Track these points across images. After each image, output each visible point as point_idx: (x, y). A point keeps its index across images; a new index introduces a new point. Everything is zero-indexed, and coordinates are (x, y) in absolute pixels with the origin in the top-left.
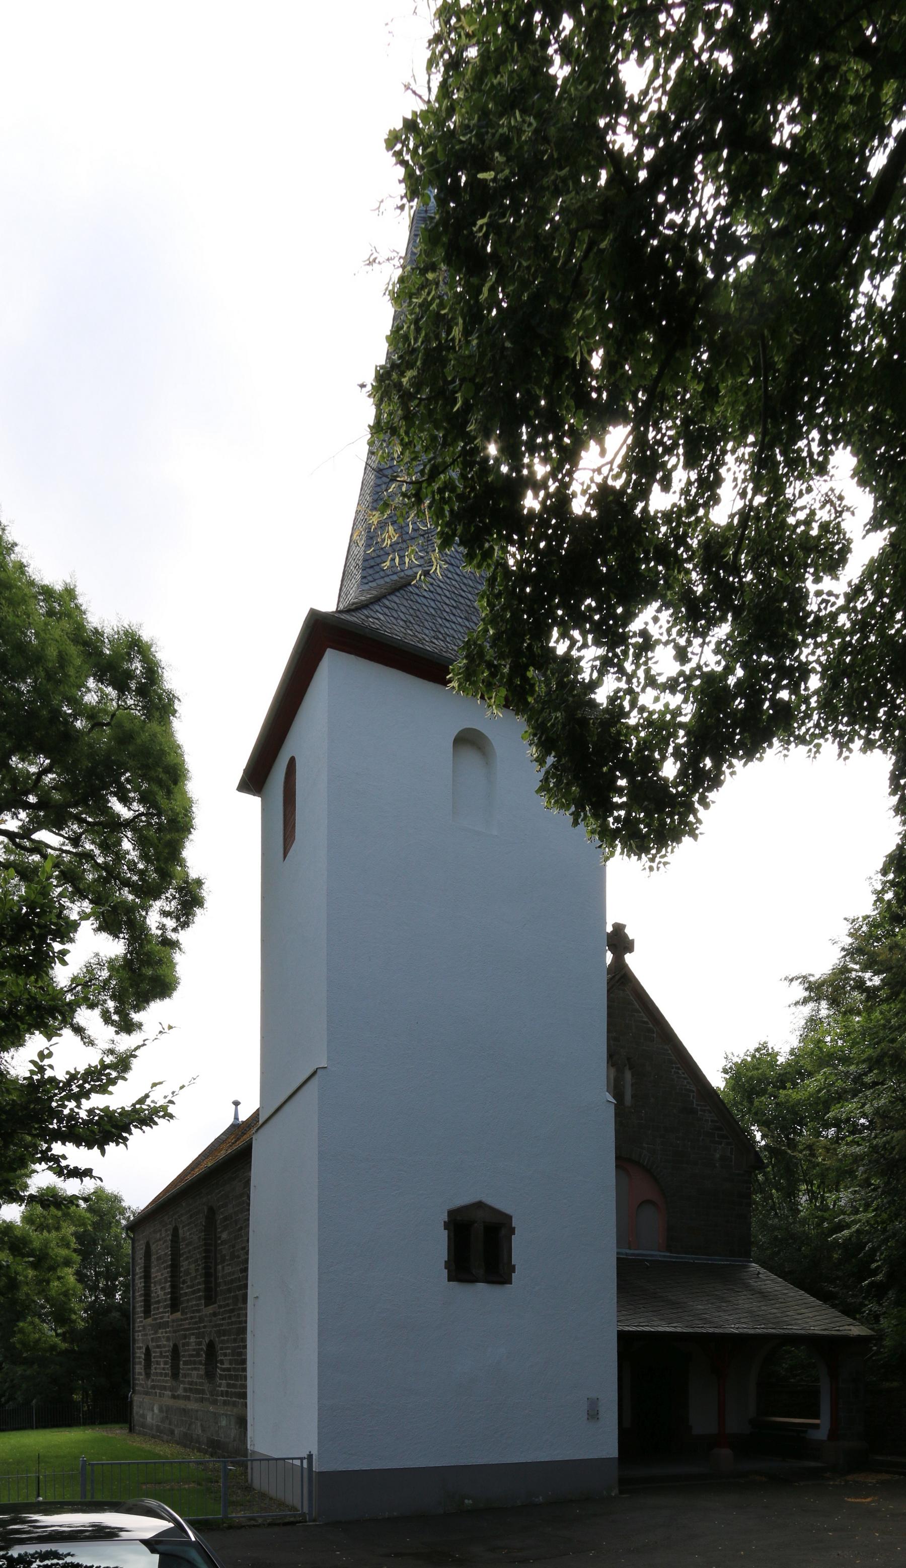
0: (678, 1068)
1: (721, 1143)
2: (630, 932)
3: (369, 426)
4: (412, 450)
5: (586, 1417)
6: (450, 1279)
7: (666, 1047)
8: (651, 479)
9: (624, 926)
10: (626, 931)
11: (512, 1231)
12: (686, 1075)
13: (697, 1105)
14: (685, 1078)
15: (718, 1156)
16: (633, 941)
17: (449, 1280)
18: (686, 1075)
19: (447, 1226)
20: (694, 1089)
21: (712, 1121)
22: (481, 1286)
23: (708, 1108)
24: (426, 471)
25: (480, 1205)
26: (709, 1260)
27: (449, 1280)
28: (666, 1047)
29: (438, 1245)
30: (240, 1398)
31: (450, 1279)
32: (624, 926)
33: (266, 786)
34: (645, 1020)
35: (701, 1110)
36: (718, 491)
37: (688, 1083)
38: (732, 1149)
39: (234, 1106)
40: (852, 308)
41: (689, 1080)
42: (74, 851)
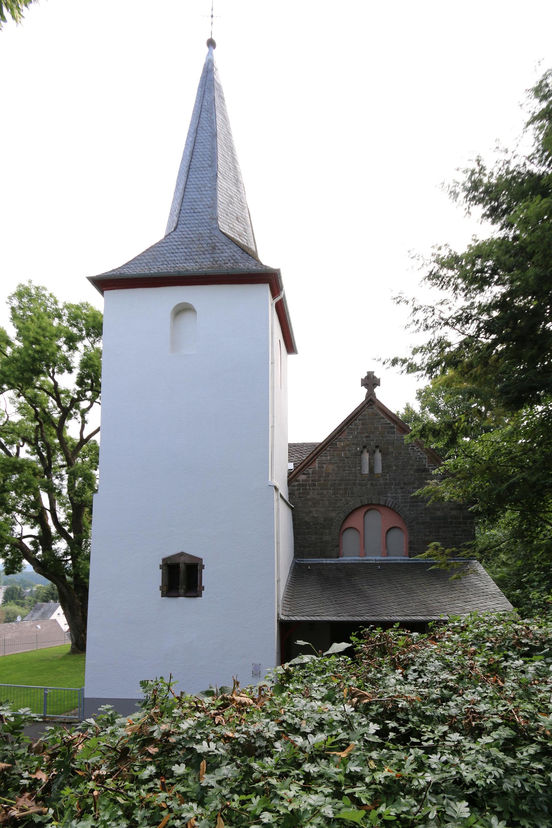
4: (455, 379)
5: (252, 675)
6: (163, 596)
9: (373, 372)
11: (203, 567)
13: (428, 466)
14: (419, 452)
16: (379, 379)
17: (162, 596)
19: (161, 567)
22: (181, 599)
24: (511, 481)
25: (182, 554)
27: (162, 596)
29: (157, 577)
31: (163, 596)
32: (373, 372)
33: (204, 69)
36: (18, 330)
37: (421, 454)
39: (206, 49)
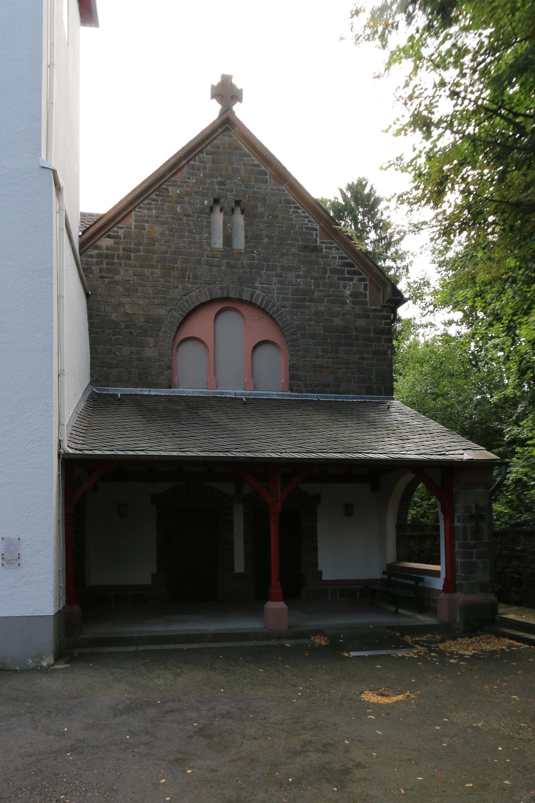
0: (298, 208)
1: (352, 280)
2: (237, 82)
3: (398, 46)
7: (281, 187)
8: (525, 310)
10: (216, 84)
12: (307, 214)
13: (321, 243)
14: (306, 217)
15: (348, 292)
18: (307, 214)
20: (318, 227)
21: (340, 258)
23: (335, 245)
26: (339, 398)
28: (281, 187)
30: (255, 191)
34: (257, 162)
35: (326, 248)
38: (365, 285)
40: (348, 652)
41: (311, 219)
42: (478, 68)
